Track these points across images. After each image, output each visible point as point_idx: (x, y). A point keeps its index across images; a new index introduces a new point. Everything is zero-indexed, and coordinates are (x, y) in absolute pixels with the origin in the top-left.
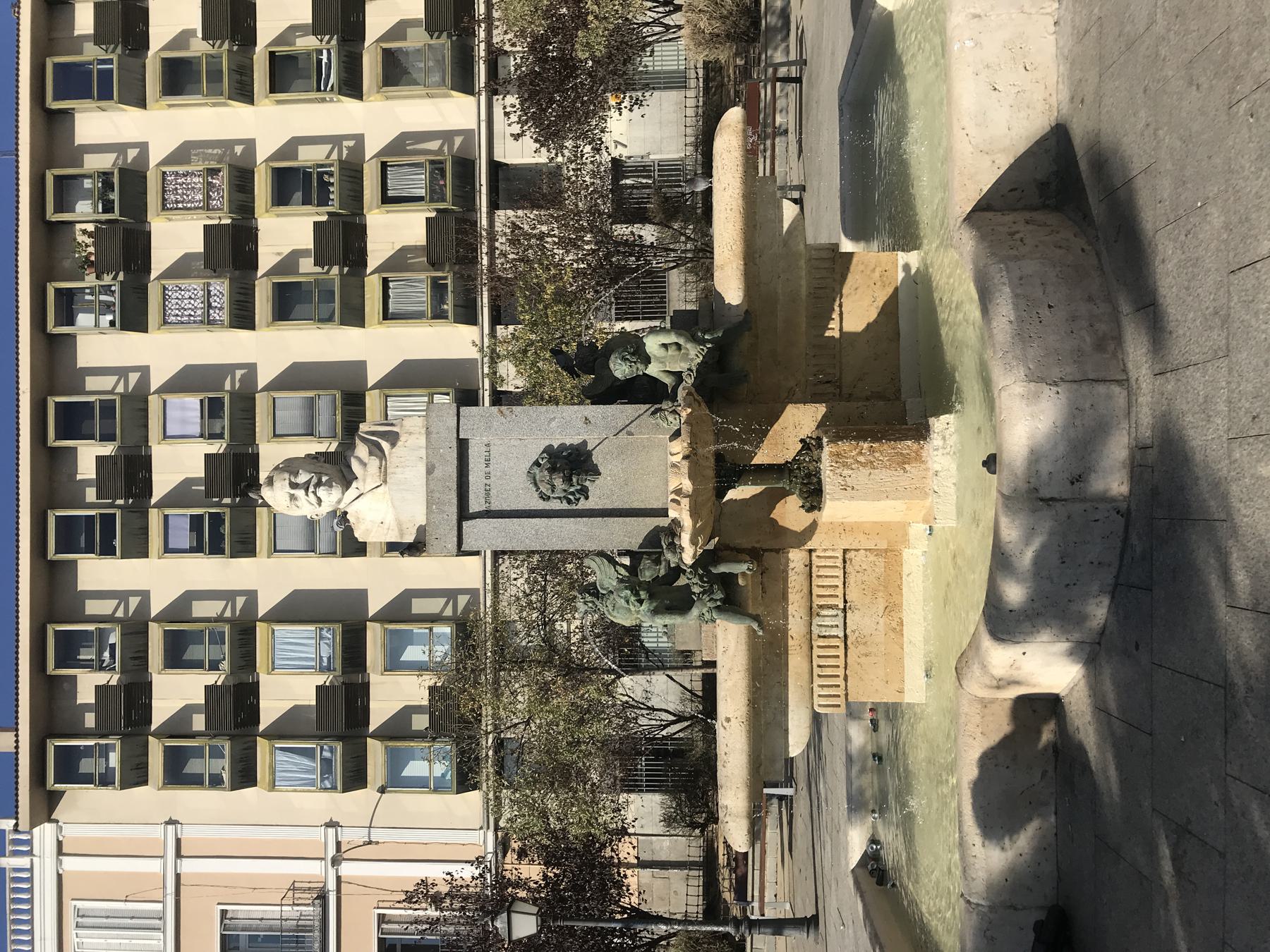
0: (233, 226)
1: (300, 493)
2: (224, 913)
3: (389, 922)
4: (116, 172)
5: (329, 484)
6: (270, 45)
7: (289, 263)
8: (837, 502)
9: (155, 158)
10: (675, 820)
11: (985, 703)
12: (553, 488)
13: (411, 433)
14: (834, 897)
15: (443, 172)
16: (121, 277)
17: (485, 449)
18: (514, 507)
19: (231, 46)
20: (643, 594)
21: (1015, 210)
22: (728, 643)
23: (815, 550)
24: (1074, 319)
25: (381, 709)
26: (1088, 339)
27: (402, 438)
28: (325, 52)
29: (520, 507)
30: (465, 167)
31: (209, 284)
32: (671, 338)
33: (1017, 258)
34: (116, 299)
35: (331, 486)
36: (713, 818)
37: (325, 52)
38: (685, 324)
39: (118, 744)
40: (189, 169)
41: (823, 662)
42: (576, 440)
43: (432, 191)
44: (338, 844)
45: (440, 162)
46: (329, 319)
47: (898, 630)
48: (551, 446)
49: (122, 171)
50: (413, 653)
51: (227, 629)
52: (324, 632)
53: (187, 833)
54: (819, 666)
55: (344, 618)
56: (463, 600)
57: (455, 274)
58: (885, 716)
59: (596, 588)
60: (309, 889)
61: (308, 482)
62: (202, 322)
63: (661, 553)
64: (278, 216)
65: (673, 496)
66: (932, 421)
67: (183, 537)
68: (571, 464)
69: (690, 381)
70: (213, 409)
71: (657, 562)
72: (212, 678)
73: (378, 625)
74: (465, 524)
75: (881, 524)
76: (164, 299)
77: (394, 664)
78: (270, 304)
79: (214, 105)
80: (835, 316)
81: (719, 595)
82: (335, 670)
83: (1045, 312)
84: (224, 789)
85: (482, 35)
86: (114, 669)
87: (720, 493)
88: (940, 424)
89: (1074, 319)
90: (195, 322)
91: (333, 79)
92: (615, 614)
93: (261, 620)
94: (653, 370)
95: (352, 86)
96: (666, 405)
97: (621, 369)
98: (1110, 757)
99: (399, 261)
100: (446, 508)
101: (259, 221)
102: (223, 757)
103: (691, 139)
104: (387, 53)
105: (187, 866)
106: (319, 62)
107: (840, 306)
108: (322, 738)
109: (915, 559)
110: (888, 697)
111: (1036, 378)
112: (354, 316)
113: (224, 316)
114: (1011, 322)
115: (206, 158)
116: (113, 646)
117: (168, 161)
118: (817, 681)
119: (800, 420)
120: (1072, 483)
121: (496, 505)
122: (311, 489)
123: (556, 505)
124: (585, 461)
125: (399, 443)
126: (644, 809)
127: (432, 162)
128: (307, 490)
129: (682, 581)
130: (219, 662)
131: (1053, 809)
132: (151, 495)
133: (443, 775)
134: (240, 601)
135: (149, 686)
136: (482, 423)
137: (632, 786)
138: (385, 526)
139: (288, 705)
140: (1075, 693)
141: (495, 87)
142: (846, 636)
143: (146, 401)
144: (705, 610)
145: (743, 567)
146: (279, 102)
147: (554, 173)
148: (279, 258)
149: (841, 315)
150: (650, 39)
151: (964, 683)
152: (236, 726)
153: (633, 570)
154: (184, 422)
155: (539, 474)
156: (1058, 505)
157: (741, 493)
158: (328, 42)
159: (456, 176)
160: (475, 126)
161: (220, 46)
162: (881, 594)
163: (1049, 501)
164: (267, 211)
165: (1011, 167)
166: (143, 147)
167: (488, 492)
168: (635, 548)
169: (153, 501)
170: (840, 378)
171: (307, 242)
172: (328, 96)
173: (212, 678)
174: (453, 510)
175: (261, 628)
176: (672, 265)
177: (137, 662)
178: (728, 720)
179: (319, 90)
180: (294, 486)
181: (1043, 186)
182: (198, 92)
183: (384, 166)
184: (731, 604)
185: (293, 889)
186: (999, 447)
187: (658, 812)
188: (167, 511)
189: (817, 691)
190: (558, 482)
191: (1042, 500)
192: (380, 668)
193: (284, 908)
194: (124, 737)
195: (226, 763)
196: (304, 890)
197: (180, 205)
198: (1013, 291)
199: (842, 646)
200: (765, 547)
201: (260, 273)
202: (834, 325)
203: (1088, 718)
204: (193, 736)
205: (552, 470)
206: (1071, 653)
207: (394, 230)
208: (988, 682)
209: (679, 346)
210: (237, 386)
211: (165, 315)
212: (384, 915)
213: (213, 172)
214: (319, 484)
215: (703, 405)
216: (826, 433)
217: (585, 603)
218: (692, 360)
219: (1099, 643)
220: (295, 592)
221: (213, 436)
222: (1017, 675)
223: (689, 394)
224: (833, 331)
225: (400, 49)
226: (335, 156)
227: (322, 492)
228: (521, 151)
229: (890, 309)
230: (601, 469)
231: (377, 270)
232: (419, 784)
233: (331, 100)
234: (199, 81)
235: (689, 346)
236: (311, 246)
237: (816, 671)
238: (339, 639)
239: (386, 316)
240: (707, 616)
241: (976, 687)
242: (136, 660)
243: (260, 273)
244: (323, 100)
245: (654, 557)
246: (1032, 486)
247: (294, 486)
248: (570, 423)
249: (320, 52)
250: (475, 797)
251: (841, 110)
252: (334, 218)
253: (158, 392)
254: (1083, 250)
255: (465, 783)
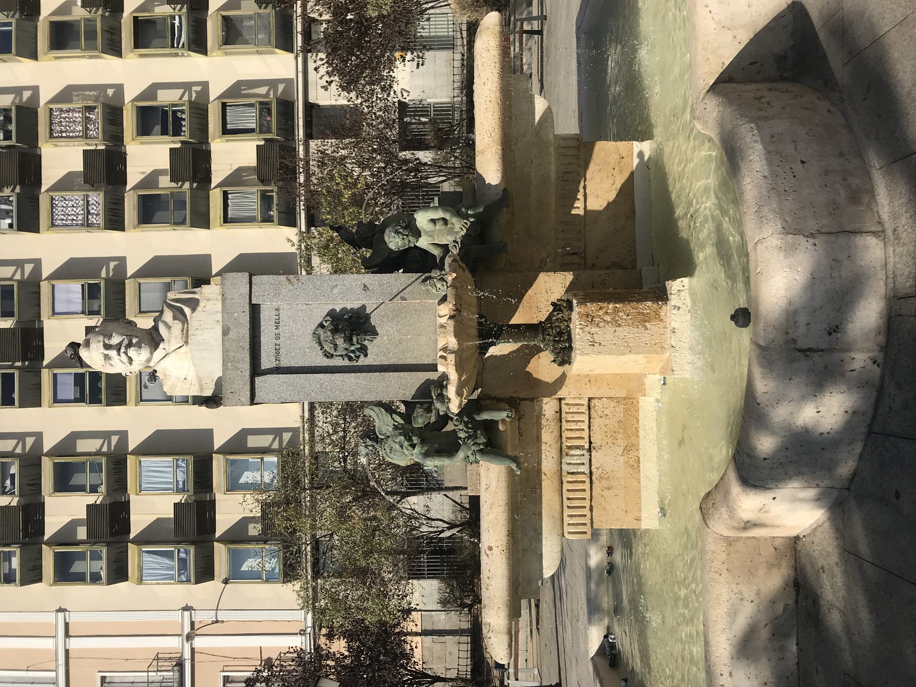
0: (106, 151)
1: (113, 353)
2: (103, 679)
3: (232, 682)
4: (13, 109)
5: (139, 346)
6: (134, 11)
7: (151, 180)
8: (586, 357)
9: (44, 97)
10: (449, 602)
11: (730, 542)
12: (336, 347)
13: (208, 300)
14: (574, 672)
15: (269, 112)
16: (18, 190)
17: (274, 313)
18: (301, 364)
19: (104, 12)
20: (415, 440)
21: (755, 82)
22: (491, 481)
23: (564, 399)
24: (827, 173)
25: (225, 519)
26: (842, 192)
27: (202, 304)
28: (177, 18)
29: (307, 363)
30: (286, 107)
31: (87, 196)
32: (439, 214)
33: (766, 119)
34: (14, 208)
35: (140, 347)
36: (478, 600)
37: (177, 18)
38: (451, 202)
39: (18, 551)
40: (71, 106)
41: (571, 495)
42: (356, 305)
43: (261, 126)
44: (192, 623)
45: (267, 103)
46: (182, 223)
47: (635, 466)
48: (333, 310)
49: (19, 108)
50: (248, 477)
51: (104, 460)
52: (180, 463)
53: (73, 618)
54: (568, 499)
55: (195, 451)
56: (287, 436)
57: (279, 187)
58: (626, 538)
59: (375, 434)
60: (170, 658)
61: (120, 344)
62: (82, 225)
63: (432, 403)
64: (142, 143)
65: (441, 353)
66: (669, 284)
67: (68, 389)
68: (352, 326)
69: (455, 252)
70: (91, 292)
71: (429, 410)
72: (92, 499)
73: (221, 456)
74: (258, 380)
75: (622, 376)
76: (52, 207)
77: (233, 486)
78: (136, 211)
79: (91, 57)
80: (580, 196)
81: (482, 440)
82: (188, 491)
83: (798, 167)
84: (102, 584)
85: (299, 10)
86: (14, 493)
87: (484, 348)
88: (678, 287)
89: (827, 173)
90: (77, 225)
91: (184, 39)
92: (392, 455)
93: (131, 454)
94: (423, 243)
95: (199, 44)
96: (435, 273)
97: (394, 242)
98: (861, 599)
99: (236, 178)
100: (240, 366)
101: (128, 147)
102: (101, 558)
103: (457, 85)
104: (226, 19)
105: (74, 644)
106: (173, 25)
107: (585, 188)
108: (179, 543)
109: (648, 405)
110: (627, 524)
111: (793, 229)
112: (202, 220)
113: (100, 220)
114: (765, 177)
115: (85, 98)
116: (13, 476)
117: (53, 101)
118: (567, 512)
119: (550, 287)
120: (830, 334)
121: (285, 363)
122: (123, 349)
123: (338, 362)
124: (364, 323)
125: (199, 309)
126: (425, 593)
127: (261, 103)
128: (119, 351)
129: (450, 427)
130: (98, 486)
131: (795, 641)
132: (43, 359)
133: (273, 569)
134: (115, 439)
135: (42, 505)
136: (270, 291)
137: (419, 576)
138: (189, 382)
139: (153, 518)
140: (818, 534)
141: (309, 46)
142: (591, 473)
143: (39, 286)
144: (469, 453)
145: (503, 415)
146: (141, 56)
147: (355, 110)
148: (143, 176)
149: (585, 196)
150: (425, 6)
151: (711, 523)
152: (112, 535)
153: (408, 417)
154: (69, 302)
155: (325, 335)
156: (815, 356)
157: (501, 349)
158: (180, 10)
159: (279, 114)
160: (294, 76)
161: (96, 12)
162: (620, 436)
163: (806, 352)
164: (133, 140)
165: (751, 42)
166: (35, 90)
167: (277, 351)
168: (409, 399)
169: (45, 363)
170: (585, 251)
171: (164, 163)
172: (180, 52)
173: (92, 499)
174: (246, 367)
175: (131, 460)
176: (444, 178)
177: (32, 488)
178: (490, 548)
179: (173, 46)
180: (107, 347)
181: (781, 59)
182: (78, 47)
183: (224, 106)
184: (493, 447)
185: (157, 659)
186: (752, 299)
187: (436, 596)
188: (56, 371)
189: (567, 520)
190: (340, 342)
191: (799, 350)
192: (223, 489)
193: (150, 674)
194: (23, 546)
195: (103, 563)
196: (166, 660)
197: (64, 135)
198: (765, 148)
199: (588, 481)
200: (522, 396)
201: (128, 187)
202: (579, 204)
203: (834, 558)
204: (77, 543)
205: (335, 331)
206: (818, 499)
207: (232, 155)
208: (736, 525)
209: (445, 221)
210: (111, 274)
211: (52, 219)
212: (228, 676)
213: (90, 109)
214: (130, 345)
215: (467, 272)
216: (575, 296)
217: (366, 447)
218: (457, 233)
219: (848, 489)
220: (157, 431)
221: (92, 313)
222: (763, 517)
223: (454, 261)
224: (578, 209)
225: (236, 16)
226: (186, 98)
227: (132, 352)
228: (328, 94)
229: (627, 191)
230: (378, 330)
231: (219, 185)
232: (253, 576)
233: (183, 55)
234: (79, 39)
235: (454, 220)
236: (168, 167)
237: (566, 503)
238: (191, 467)
239: (226, 220)
240: (472, 458)
241: (721, 526)
242: (32, 486)
243: (128, 188)
244: (177, 55)
245: (426, 406)
246: (791, 336)
247: (107, 347)
248: (356, 290)
249: (173, 18)
250: (297, 585)
251: (578, 39)
252: (185, 146)
253: (48, 279)
254: (829, 111)
255: (289, 573)
